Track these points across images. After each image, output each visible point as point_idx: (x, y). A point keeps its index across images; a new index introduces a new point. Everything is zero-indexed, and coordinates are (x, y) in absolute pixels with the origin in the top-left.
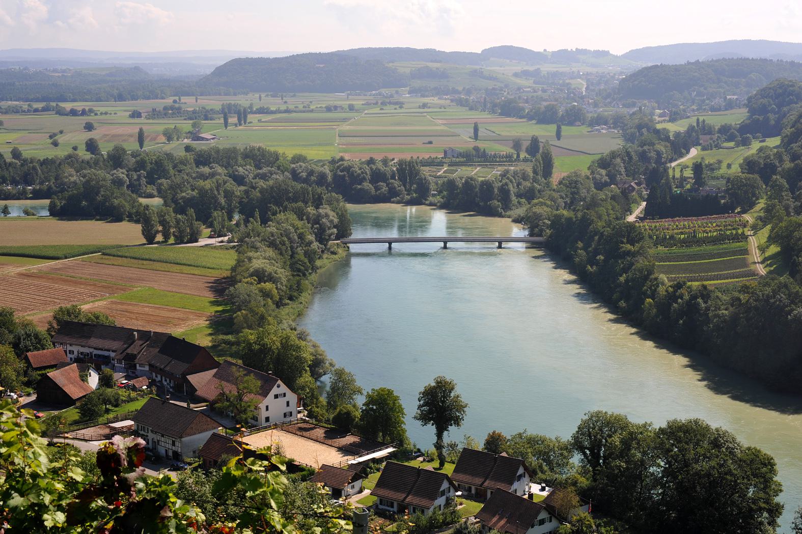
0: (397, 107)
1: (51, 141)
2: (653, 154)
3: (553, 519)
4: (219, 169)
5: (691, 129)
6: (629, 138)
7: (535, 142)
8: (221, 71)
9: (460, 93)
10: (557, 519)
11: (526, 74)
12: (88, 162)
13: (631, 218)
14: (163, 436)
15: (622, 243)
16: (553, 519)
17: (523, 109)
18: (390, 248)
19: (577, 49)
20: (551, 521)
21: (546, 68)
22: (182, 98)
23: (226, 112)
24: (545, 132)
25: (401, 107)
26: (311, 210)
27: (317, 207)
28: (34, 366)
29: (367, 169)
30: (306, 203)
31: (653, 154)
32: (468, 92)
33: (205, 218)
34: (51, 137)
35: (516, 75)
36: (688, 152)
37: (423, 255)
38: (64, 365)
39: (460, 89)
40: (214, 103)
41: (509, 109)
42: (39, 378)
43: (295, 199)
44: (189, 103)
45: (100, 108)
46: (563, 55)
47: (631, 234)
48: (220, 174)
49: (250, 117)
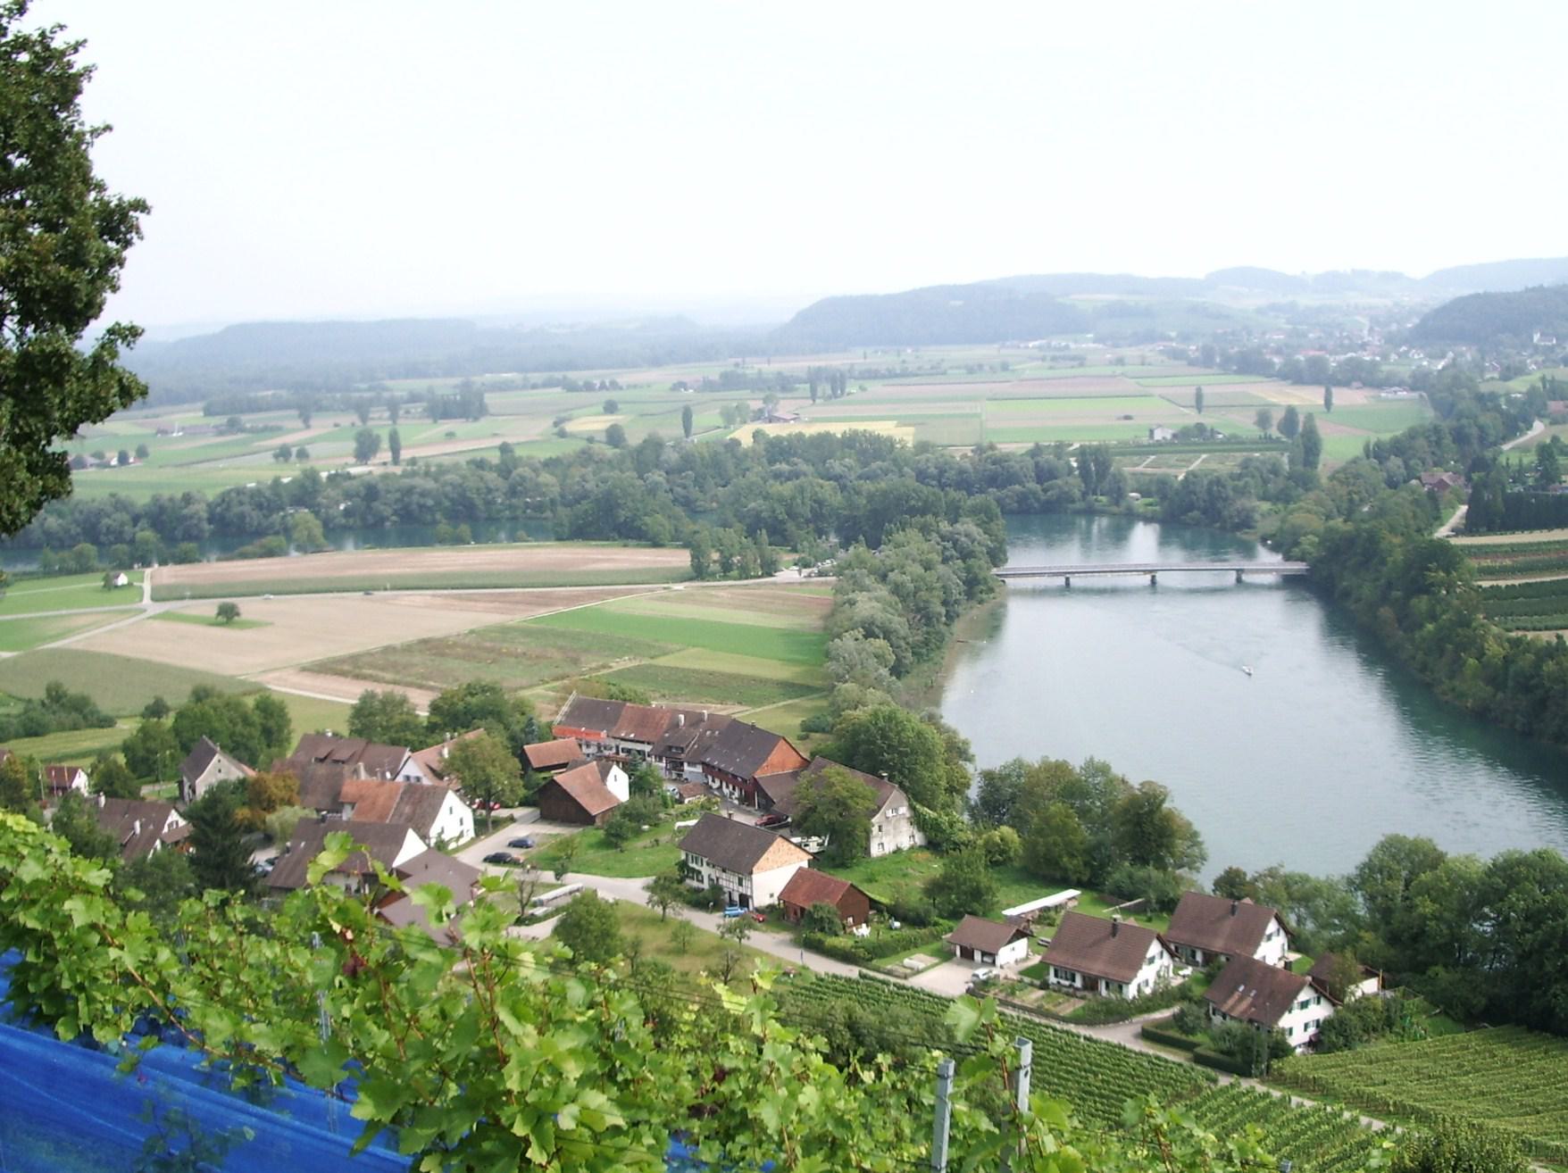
0: (1076, 363)
1: (556, 430)
2: (1474, 431)
3: (1322, 1000)
4: (803, 467)
5: (1532, 393)
6: (1437, 404)
7: (1291, 413)
8: (805, 317)
9: (1171, 339)
10: (1329, 1000)
11: (1274, 308)
12: (610, 461)
13: (1442, 532)
14: (724, 871)
15: (1429, 570)
16: (1322, 1000)
17: (1271, 364)
18: (1153, 581)
19: (1353, 270)
20: (1319, 1003)
21: (1305, 301)
22: (748, 359)
23: (814, 378)
24: (1307, 398)
25: (1081, 365)
26: (945, 526)
27: (953, 522)
28: (535, 764)
29: (1030, 462)
30: (936, 515)
31: (1474, 431)
32: (1185, 338)
33: (780, 536)
34: (556, 424)
35: (1259, 311)
36: (1530, 427)
37: (1114, 591)
38: (577, 764)
39: (1173, 334)
40: (798, 365)
41: (1250, 364)
42: (543, 783)
43: (923, 512)
44: (755, 367)
45: (624, 378)
46: (1331, 281)
47: (1443, 555)
48: (805, 474)
49: (852, 388)
